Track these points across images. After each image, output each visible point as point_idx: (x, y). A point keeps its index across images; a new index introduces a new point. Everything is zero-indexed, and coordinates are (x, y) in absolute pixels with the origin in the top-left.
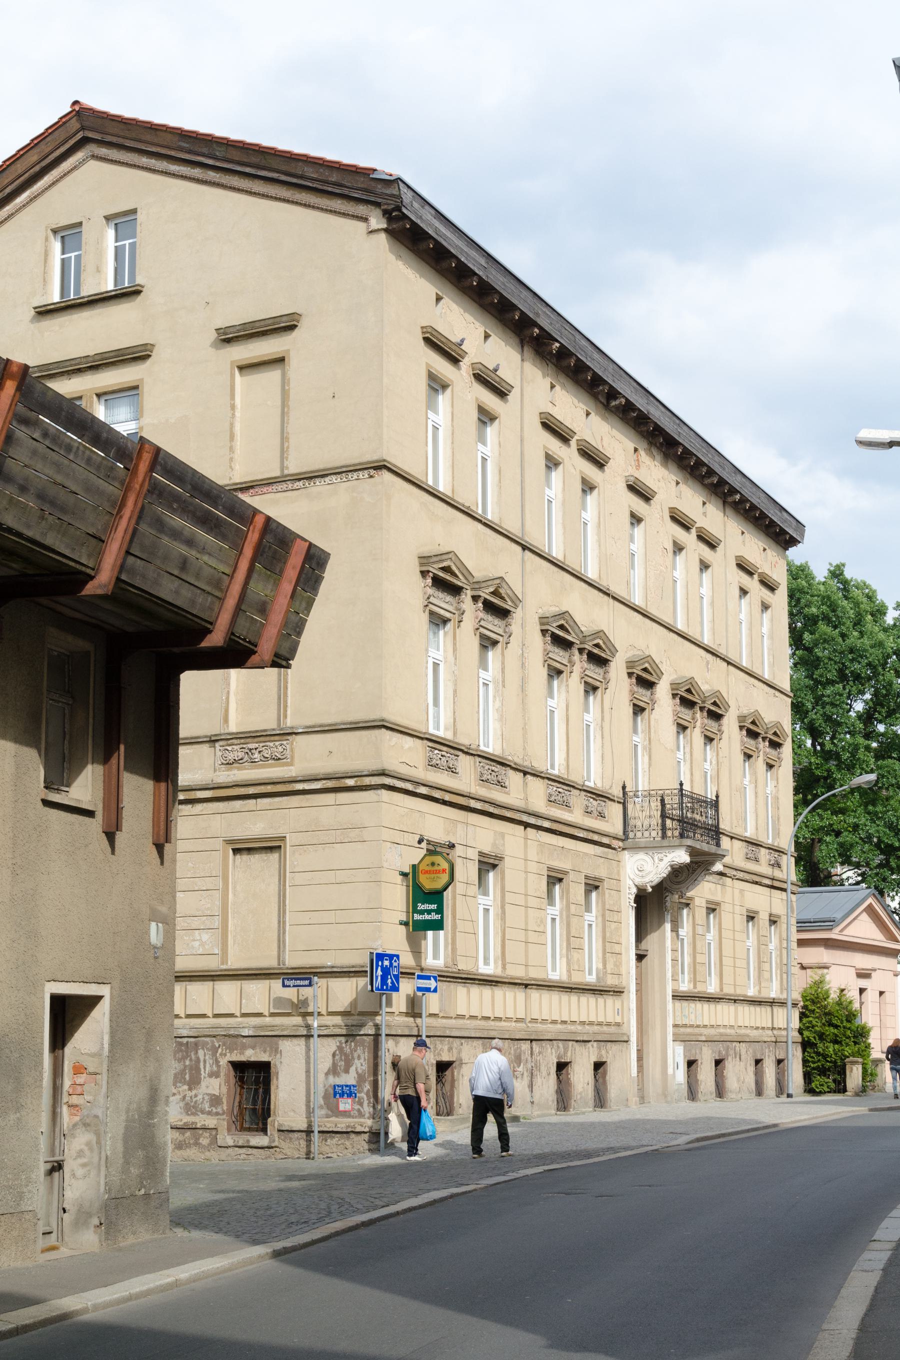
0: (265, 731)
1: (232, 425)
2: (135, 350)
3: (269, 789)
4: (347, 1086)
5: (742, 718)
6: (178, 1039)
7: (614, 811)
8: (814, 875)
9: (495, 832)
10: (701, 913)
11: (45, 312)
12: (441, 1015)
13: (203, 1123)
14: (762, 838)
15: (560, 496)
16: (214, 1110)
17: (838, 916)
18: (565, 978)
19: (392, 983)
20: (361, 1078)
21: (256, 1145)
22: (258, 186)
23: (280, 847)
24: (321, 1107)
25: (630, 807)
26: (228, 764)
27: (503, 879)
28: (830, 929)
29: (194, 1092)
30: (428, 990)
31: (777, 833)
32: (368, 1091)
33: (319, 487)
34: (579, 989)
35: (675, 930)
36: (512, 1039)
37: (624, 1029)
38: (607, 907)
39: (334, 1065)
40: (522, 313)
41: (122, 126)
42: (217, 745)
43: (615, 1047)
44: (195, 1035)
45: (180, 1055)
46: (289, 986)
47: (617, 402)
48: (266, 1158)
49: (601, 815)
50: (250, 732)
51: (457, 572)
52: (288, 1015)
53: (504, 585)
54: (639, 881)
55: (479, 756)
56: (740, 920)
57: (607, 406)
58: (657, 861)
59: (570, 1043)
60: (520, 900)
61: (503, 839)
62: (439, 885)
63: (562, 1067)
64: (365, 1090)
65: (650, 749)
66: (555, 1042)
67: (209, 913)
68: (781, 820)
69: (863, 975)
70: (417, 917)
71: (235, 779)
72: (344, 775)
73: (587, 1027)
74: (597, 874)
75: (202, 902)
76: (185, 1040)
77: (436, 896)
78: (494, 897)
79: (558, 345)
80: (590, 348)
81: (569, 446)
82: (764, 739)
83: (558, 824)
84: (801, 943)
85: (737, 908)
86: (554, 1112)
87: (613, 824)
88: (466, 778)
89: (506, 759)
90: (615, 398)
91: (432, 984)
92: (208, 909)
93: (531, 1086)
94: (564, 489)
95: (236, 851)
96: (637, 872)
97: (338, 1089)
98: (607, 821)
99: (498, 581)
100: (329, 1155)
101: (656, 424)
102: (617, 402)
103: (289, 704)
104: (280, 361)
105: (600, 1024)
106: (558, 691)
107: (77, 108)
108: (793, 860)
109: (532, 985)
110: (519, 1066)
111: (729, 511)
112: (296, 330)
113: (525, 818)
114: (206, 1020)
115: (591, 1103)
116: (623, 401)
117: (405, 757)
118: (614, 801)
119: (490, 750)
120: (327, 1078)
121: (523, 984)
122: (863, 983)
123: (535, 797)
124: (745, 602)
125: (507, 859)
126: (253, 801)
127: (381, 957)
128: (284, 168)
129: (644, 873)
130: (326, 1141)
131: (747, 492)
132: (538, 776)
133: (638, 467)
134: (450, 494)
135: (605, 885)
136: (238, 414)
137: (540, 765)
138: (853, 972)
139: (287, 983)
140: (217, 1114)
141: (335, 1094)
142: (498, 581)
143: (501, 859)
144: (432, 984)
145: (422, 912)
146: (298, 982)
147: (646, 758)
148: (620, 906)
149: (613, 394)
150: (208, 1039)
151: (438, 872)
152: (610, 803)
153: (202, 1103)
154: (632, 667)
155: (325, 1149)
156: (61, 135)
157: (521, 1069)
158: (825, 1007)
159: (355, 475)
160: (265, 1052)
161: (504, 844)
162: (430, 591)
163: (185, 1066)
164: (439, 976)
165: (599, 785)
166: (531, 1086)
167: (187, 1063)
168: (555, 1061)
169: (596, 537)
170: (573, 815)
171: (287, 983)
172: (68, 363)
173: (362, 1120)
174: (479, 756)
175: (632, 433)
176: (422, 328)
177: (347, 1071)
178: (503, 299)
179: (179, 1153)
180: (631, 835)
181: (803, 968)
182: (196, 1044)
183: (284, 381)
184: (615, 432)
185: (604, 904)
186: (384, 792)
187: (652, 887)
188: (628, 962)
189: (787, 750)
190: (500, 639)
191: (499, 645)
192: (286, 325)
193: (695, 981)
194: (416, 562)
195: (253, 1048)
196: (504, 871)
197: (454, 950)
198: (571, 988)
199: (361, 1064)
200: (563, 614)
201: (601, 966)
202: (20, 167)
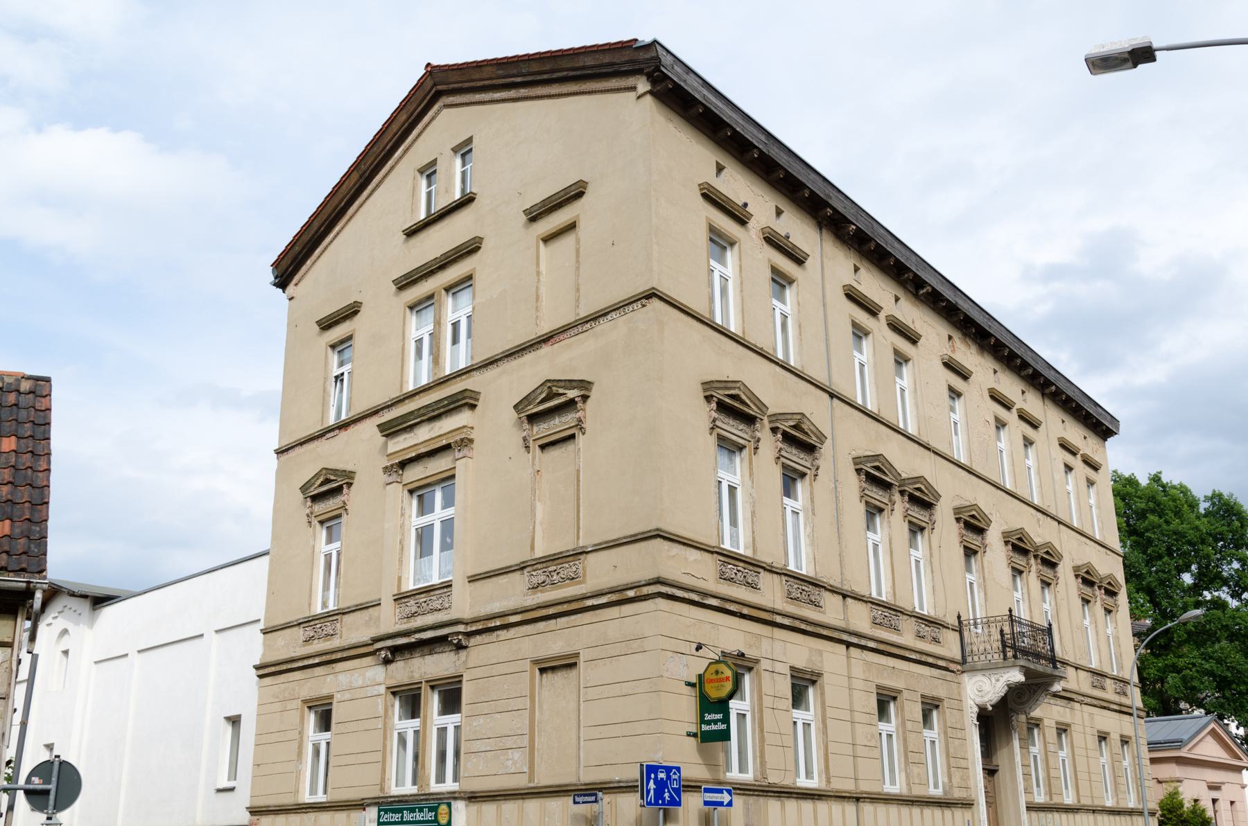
5: (1076, 569)
7: (951, 638)
8: (1161, 703)
9: (811, 649)
10: (1051, 734)
11: (411, 233)
14: (1107, 670)
15: (871, 360)
17: (1185, 737)
18: (905, 792)
19: (671, 796)
22: (555, 89)
25: (966, 634)
27: (823, 694)
28: (1179, 748)
30: (721, 804)
31: (1121, 667)
33: (603, 325)
35: (1025, 745)
40: (812, 192)
41: (459, 72)
49: (936, 640)
54: (979, 701)
55: (786, 575)
56: (1092, 741)
57: (916, 296)
61: (821, 655)
67: (519, 732)
68: (1124, 656)
69: (1214, 787)
70: (705, 728)
74: (935, 694)
77: (722, 706)
80: (889, 237)
82: (1100, 588)
84: (1153, 761)
85: (1088, 730)
87: (950, 646)
88: (771, 594)
91: (726, 798)
95: (543, 671)
104: (572, 227)
108: (1138, 690)
111: (1049, 404)
112: (585, 197)
113: (845, 637)
117: (698, 571)
119: (804, 572)
122: (1215, 794)
124: (1070, 477)
125: (825, 675)
126: (553, 621)
127: (652, 769)
128: (570, 65)
131: (1062, 385)
133: (953, 351)
135: (946, 704)
137: (860, 590)
138: (1204, 785)
139: (577, 799)
143: (820, 675)
145: (709, 723)
146: (587, 799)
147: (982, 594)
149: (1025, 365)
151: (721, 680)
156: (420, 94)
158: (1181, 815)
170: (890, 634)
171: (577, 799)
174: (786, 575)
180: (969, 659)
181: (1160, 782)
183: (578, 241)
185: (945, 721)
186: (660, 601)
188: (975, 775)
189: (1123, 598)
192: (575, 193)
193: (1050, 793)
194: (700, 388)
197: (763, 763)
201: (946, 780)
202: (395, 127)
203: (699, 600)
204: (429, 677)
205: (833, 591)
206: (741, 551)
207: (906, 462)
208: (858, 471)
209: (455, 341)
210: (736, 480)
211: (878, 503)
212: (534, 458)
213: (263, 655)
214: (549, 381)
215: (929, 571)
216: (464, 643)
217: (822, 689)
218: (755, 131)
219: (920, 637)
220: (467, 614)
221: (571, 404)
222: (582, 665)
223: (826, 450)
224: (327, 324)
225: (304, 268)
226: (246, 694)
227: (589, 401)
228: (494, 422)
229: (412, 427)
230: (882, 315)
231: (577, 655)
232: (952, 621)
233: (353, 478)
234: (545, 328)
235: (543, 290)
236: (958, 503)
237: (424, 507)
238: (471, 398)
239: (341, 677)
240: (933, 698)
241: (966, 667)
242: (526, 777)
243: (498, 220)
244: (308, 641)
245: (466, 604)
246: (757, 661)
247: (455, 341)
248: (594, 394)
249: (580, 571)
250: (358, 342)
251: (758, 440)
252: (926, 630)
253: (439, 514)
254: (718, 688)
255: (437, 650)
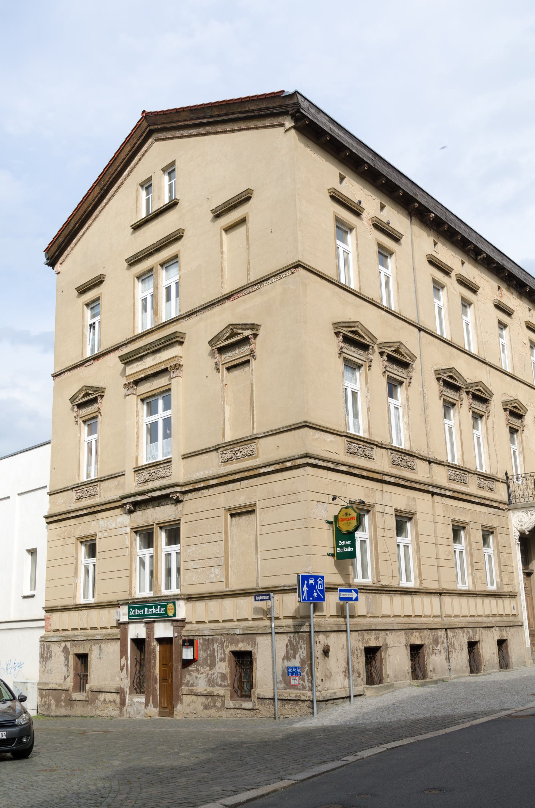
0: (242, 438)
1: (222, 263)
2: (175, 234)
3: (246, 474)
4: (295, 667)
6: (204, 637)
9: (408, 497)
12: (369, 615)
13: (217, 692)
15: (446, 305)
16: (223, 684)
18: (471, 588)
19: (318, 595)
20: (303, 662)
21: (246, 708)
22: (229, 127)
23: (254, 510)
24: (281, 682)
25: (511, 485)
26: (225, 462)
27: (416, 526)
29: (213, 671)
30: (351, 599)
32: (307, 670)
33: (266, 286)
34: (483, 594)
36: (429, 629)
37: (519, 618)
38: (500, 544)
39: (287, 653)
40: (404, 192)
42: (219, 451)
43: (513, 630)
44: (211, 634)
45: (204, 647)
46: (258, 600)
47: (482, 257)
48: (252, 717)
49: (491, 490)
50: (235, 440)
51: (363, 335)
52: (261, 619)
53: (402, 346)
54: (520, 528)
58: (529, 515)
59: (478, 629)
60: (432, 540)
61: (415, 501)
62: (351, 527)
63: (472, 645)
64: (306, 670)
65: (523, 453)
66: (465, 629)
70: (339, 550)
71: (228, 470)
72: (285, 460)
73: (491, 618)
74: (491, 524)
75: (215, 549)
76: (207, 638)
77: (350, 536)
78: (412, 538)
79: (433, 215)
81: (450, 277)
83: (457, 494)
86: (467, 674)
87: (500, 493)
88: (381, 462)
89: (413, 452)
90: (480, 255)
91: (354, 595)
92: (218, 553)
93: (448, 659)
94: (448, 301)
95: (232, 515)
96: (519, 523)
97: (290, 670)
98: (496, 493)
99: (398, 344)
100: (287, 716)
101: (509, 272)
102: (482, 257)
103: (255, 420)
104: (243, 221)
105: (501, 616)
106: (454, 416)
107: (144, 114)
109: (445, 593)
110: (437, 647)
112: (251, 200)
113: (431, 489)
114: (97, 630)
115: (498, 666)
116: (485, 255)
118: (499, 481)
119: (403, 447)
120: (283, 662)
121: (437, 593)
123: (440, 477)
126: (238, 483)
127: (305, 578)
129: (522, 523)
130: (285, 706)
132: (440, 464)
133: (501, 297)
134: (358, 290)
135: (498, 531)
136: (225, 256)
137: (441, 458)
139: (257, 598)
140: (225, 686)
141: (288, 673)
142: (398, 344)
143: (414, 514)
144: (354, 595)
145: (342, 547)
147: (522, 458)
148: (510, 543)
150: (219, 637)
151: (349, 519)
152: (497, 482)
153: (217, 679)
154: (506, 405)
155: (285, 712)
156: (139, 132)
157: (439, 647)
159: (284, 274)
160: (249, 644)
161: (416, 505)
162: (342, 344)
163: (208, 655)
164: (359, 589)
165: (489, 472)
166: (448, 659)
167: (209, 652)
168: (467, 641)
169: (475, 331)
171: (257, 598)
172: (145, 251)
173: (304, 692)
175: (496, 278)
176: (328, 190)
177: (294, 657)
178: (388, 180)
179: (206, 711)
180: (513, 501)
182: (213, 640)
183: (248, 230)
184: (483, 275)
186: (309, 469)
187: (528, 531)
190: (405, 380)
191: (404, 384)
192: (244, 198)
194: (331, 327)
195: (243, 642)
196: (417, 522)
197: (378, 572)
198: (476, 594)
199: (302, 653)
200: (451, 369)
201: (499, 580)
202: (123, 155)
203: (334, 467)
204: (158, 521)
205: (423, 459)
206: (361, 434)
207: (470, 372)
208: (438, 379)
209: (168, 299)
210: (357, 387)
211: (451, 400)
212: (223, 376)
213: (50, 509)
214: (231, 325)
215: (486, 444)
216: (180, 498)
217: (416, 523)
218: (365, 152)
219: (481, 487)
220: (181, 479)
221: (246, 340)
222: (258, 511)
223: (416, 365)
224: (83, 290)
225: (66, 253)
226: (40, 535)
227: (258, 337)
228: (195, 353)
229: (141, 358)
230: (453, 274)
231: (254, 505)
232: (502, 476)
233: (104, 392)
234: (227, 289)
235: (225, 264)
236: (505, 398)
237: (152, 411)
238: (180, 337)
239: (101, 522)
240: (490, 527)
241: (512, 506)
242: (223, 584)
243: (193, 217)
244: (79, 499)
245: (180, 473)
246: (373, 506)
247: (168, 299)
248: (261, 333)
249: (255, 450)
250: (104, 301)
251: (371, 361)
252: (485, 483)
253: (161, 414)
254: (347, 525)
255: (163, 503)
